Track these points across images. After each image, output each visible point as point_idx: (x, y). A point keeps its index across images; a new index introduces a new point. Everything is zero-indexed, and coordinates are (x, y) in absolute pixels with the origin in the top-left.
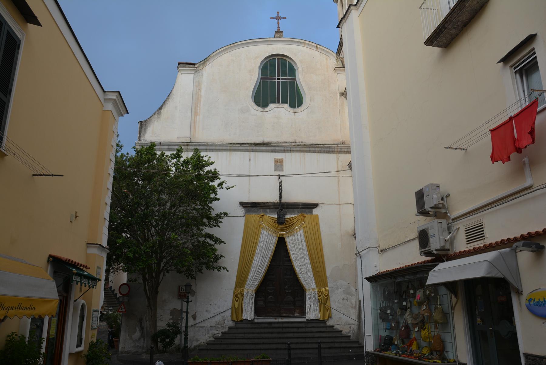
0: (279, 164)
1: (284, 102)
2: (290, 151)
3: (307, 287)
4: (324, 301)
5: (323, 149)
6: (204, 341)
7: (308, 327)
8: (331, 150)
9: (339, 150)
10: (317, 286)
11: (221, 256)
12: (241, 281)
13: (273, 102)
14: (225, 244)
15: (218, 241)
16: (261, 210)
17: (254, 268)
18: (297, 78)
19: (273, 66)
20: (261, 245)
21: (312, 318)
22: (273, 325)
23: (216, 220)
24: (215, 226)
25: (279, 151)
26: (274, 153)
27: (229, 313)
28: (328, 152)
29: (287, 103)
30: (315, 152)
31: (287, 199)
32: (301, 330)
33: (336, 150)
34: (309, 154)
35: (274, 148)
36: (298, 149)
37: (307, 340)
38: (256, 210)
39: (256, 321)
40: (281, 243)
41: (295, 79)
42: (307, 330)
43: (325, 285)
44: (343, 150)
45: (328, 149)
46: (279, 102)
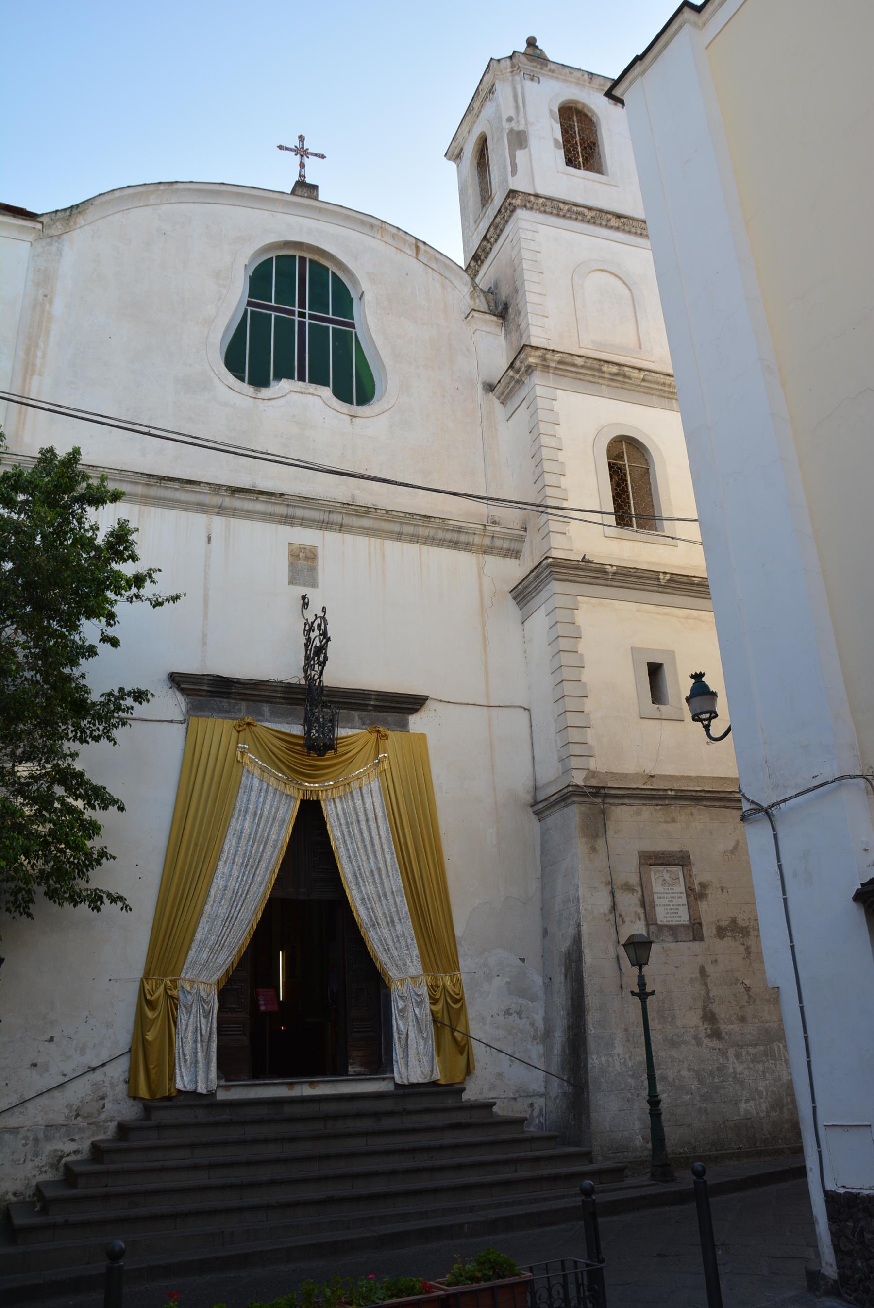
0: (303, 565)
1: (319, 379)
2: (341, 528)
3: (392, 973)
4: (448, 1020)
5: (440, 535)
6: (19, 1186)
7: (409, 1113)
8: (463, 538)
9: (487, 541)
10: (425, 970)
11: (103, 854)
12: (167, 949)
13: (284, 373)
14: (121, 809)
15: (99, 797)
16: (243, 705)
17: (216, 906)
18: (357, 321)
19: (285, 276)
20: (241, 825)
21: (414, 1080)
22: (288, 1110)
23: (107, 715)
24: (97, 739)
25: (303, 522)
26: (287, 528)
27: (118, 1071)
28: (455, 545)
29: (327, 385)
30: (415, 539)
31: (336, 675)
32: (387, 1123)
33: (477, 540)
34: (397, 544)
35: (291, 511)
36: (365, 522)
37: (422, 1161)
38: (225, 703)
39: (222, 1095)
40: (310, 815)
41: (352, 326)
42: (409, 1122)
43: (452, 965)
44: (498, 543)
45: (455, 536)
46: (302, 378)
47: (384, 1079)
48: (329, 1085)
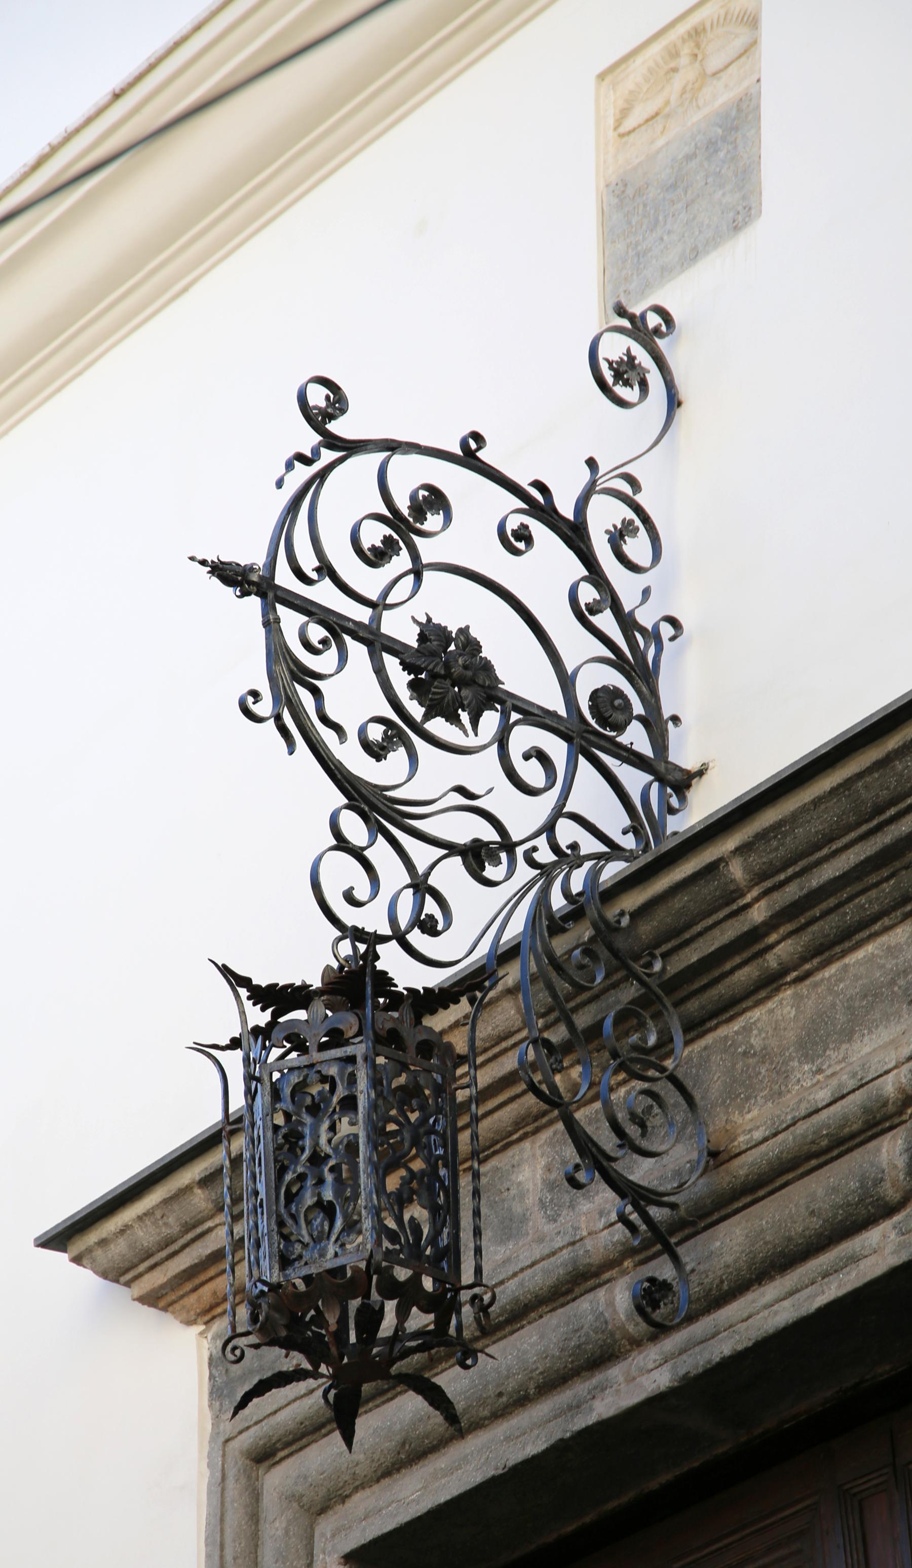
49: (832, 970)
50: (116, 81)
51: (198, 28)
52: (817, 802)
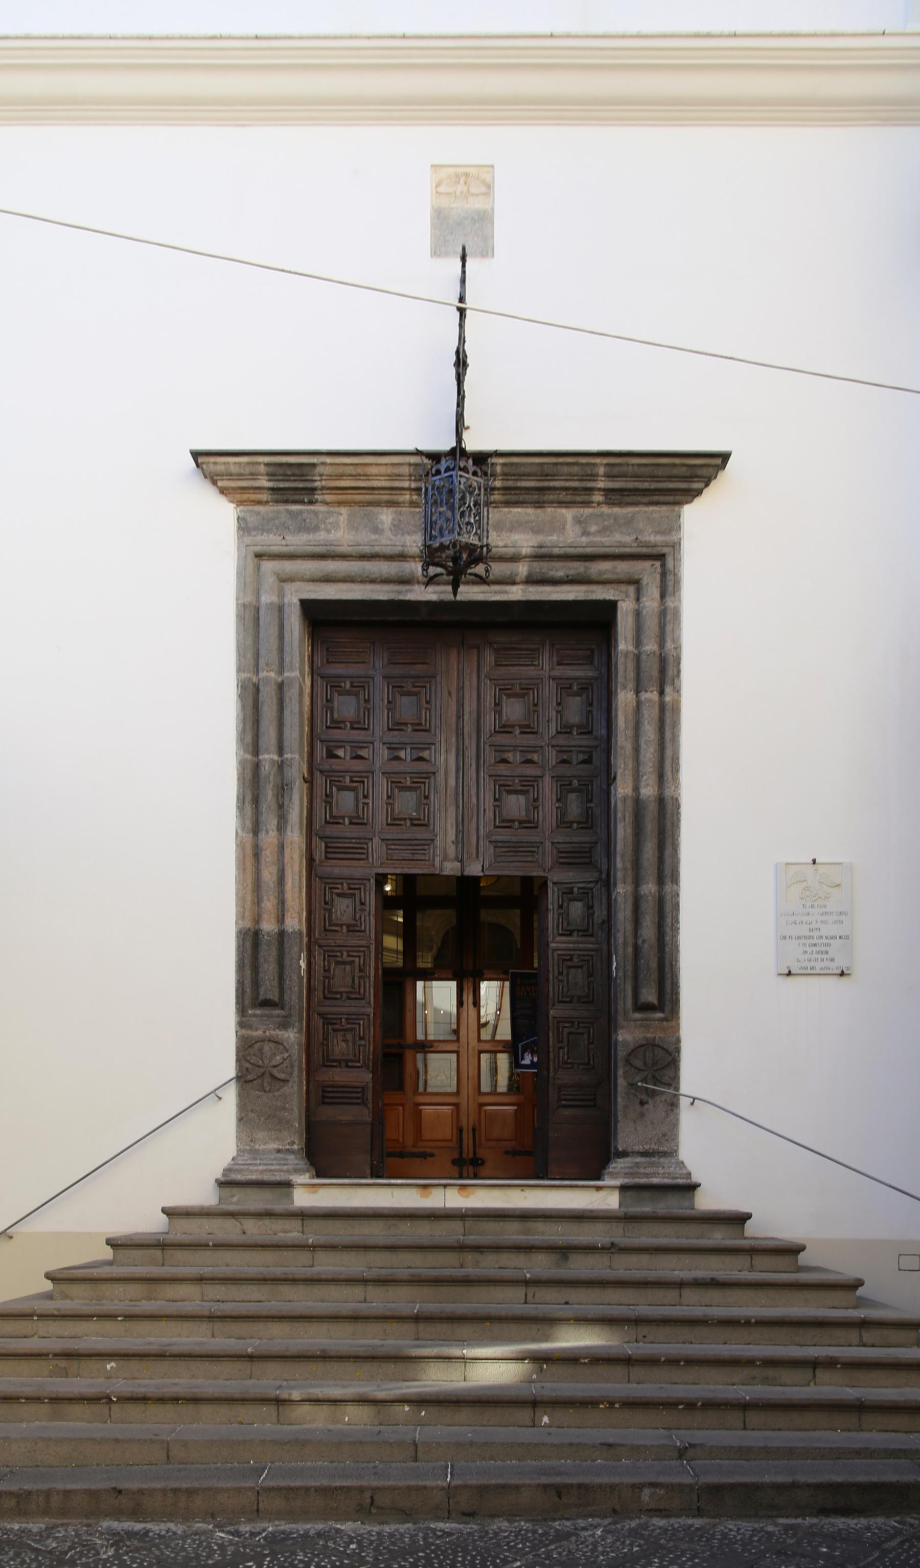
47: (599, 1188)
48: (496, 1193)
49: (506, 510)
50: (261, 32)
51: (300, 38)
52: (532, 464)
